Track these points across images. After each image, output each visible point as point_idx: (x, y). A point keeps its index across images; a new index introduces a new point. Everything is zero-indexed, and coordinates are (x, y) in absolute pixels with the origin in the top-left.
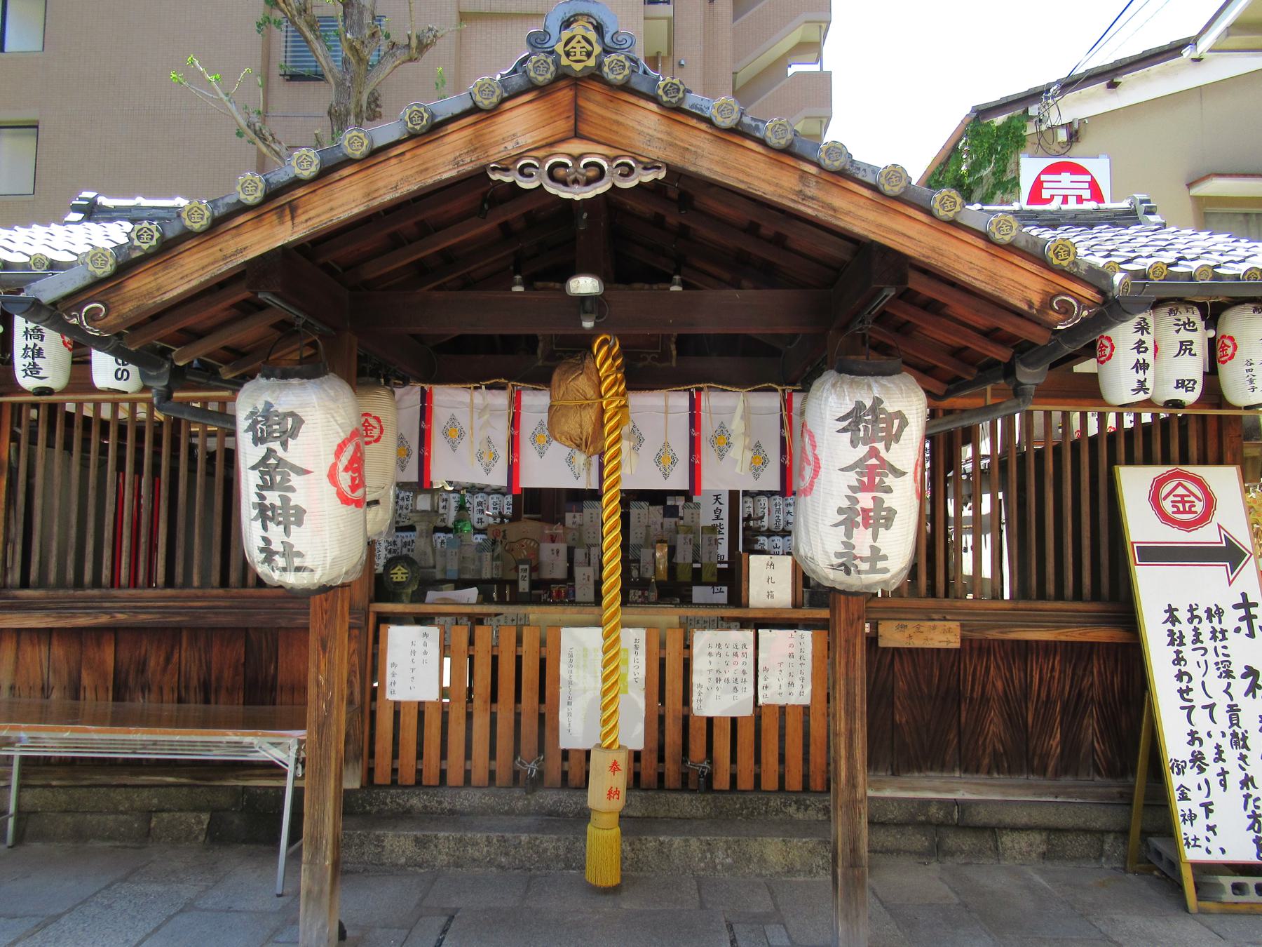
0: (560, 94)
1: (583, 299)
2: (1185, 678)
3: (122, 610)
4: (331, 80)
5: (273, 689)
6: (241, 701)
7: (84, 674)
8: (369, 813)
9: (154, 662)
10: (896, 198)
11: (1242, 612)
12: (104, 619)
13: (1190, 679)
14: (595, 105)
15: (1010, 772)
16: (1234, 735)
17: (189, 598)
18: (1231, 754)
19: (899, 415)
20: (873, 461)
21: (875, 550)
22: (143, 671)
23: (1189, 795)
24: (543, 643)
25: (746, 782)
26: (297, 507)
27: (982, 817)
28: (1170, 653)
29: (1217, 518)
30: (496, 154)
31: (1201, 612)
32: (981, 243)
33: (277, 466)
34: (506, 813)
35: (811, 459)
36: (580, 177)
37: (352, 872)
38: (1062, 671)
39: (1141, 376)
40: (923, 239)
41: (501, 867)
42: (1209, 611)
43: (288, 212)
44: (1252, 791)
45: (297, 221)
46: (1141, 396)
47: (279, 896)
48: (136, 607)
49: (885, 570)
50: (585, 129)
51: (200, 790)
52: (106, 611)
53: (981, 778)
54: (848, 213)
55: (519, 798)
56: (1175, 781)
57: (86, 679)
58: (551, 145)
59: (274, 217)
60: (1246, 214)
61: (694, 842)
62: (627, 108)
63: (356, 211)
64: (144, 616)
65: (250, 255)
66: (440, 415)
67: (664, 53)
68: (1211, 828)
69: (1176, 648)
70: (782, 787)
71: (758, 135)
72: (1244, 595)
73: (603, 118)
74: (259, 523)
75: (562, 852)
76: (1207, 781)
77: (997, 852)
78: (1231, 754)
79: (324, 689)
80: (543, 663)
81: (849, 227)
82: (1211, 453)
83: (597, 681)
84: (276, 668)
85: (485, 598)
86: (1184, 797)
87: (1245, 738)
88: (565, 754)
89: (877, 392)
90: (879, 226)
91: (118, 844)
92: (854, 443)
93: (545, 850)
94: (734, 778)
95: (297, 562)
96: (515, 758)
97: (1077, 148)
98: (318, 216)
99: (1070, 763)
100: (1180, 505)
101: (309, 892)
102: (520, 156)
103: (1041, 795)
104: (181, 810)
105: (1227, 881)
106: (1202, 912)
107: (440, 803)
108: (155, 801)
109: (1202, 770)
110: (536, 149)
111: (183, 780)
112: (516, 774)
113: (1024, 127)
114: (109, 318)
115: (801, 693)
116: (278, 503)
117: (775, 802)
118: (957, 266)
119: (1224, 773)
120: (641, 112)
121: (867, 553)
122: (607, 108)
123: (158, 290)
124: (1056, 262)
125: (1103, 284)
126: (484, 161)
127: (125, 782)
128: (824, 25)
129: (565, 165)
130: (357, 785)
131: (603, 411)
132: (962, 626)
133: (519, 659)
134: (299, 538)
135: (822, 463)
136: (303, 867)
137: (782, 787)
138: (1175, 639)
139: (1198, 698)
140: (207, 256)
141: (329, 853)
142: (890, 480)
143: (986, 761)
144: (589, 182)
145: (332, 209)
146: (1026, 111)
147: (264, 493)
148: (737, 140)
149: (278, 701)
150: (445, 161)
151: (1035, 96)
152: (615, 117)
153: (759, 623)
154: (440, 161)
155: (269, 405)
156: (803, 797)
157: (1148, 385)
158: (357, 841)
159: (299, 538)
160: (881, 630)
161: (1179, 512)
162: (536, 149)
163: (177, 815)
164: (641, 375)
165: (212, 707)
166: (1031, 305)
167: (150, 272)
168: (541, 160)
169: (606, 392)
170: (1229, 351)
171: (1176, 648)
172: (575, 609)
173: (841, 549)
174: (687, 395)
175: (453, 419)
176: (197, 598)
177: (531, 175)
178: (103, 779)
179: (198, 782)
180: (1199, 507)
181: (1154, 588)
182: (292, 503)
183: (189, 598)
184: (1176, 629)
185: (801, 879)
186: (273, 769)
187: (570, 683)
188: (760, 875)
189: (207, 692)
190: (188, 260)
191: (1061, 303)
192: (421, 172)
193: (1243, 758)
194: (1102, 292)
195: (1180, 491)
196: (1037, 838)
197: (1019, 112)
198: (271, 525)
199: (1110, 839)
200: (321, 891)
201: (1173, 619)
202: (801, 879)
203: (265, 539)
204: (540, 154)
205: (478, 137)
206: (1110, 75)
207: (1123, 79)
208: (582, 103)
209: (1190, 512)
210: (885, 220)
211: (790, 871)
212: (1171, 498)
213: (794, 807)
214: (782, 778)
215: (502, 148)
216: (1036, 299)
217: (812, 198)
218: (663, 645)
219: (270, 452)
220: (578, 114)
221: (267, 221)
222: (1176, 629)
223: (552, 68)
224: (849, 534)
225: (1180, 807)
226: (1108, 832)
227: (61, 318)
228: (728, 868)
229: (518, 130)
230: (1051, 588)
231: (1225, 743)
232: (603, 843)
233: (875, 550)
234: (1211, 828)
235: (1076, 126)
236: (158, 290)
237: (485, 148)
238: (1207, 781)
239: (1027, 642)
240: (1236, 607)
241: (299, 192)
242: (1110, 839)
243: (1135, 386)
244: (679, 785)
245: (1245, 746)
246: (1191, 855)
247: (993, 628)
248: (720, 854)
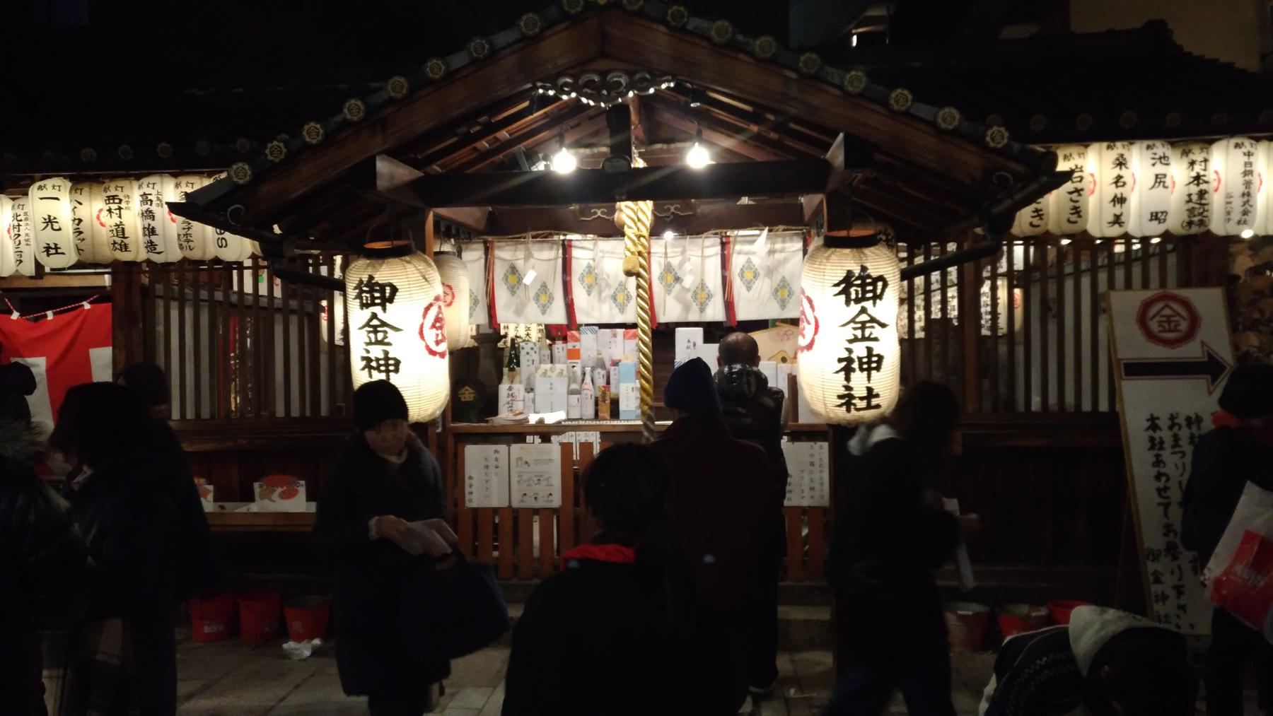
2: (1164, 479)
13: (1168, 480)
19: (881, 278)
21: (870, 390)
23: (1163, 579)
28: (1150, 456)
29: (1202, 335)
31: (1181, 420)
49: (878, 406)
56: (1151, 566)
69: (1155, 452)
76: (1180, 568)
92: (848, 302)
100: (1166, 325)
110: (571, 67)
121: (864, 394)
142: (877, 331)
161: (1164, 331)
162: (571, 67)
171: (1155, 452)
180: (1184, 326)
184: (1158, 435)
195: (1167, 312)
209: (1175, 330)
212: (1158, 318)
219: (374, 316)
222: (1158, 435)
224: (848, 379)
225: (1156, 589)
233: (870, 390)
238: (1180, 568)
243: (1111, 219)
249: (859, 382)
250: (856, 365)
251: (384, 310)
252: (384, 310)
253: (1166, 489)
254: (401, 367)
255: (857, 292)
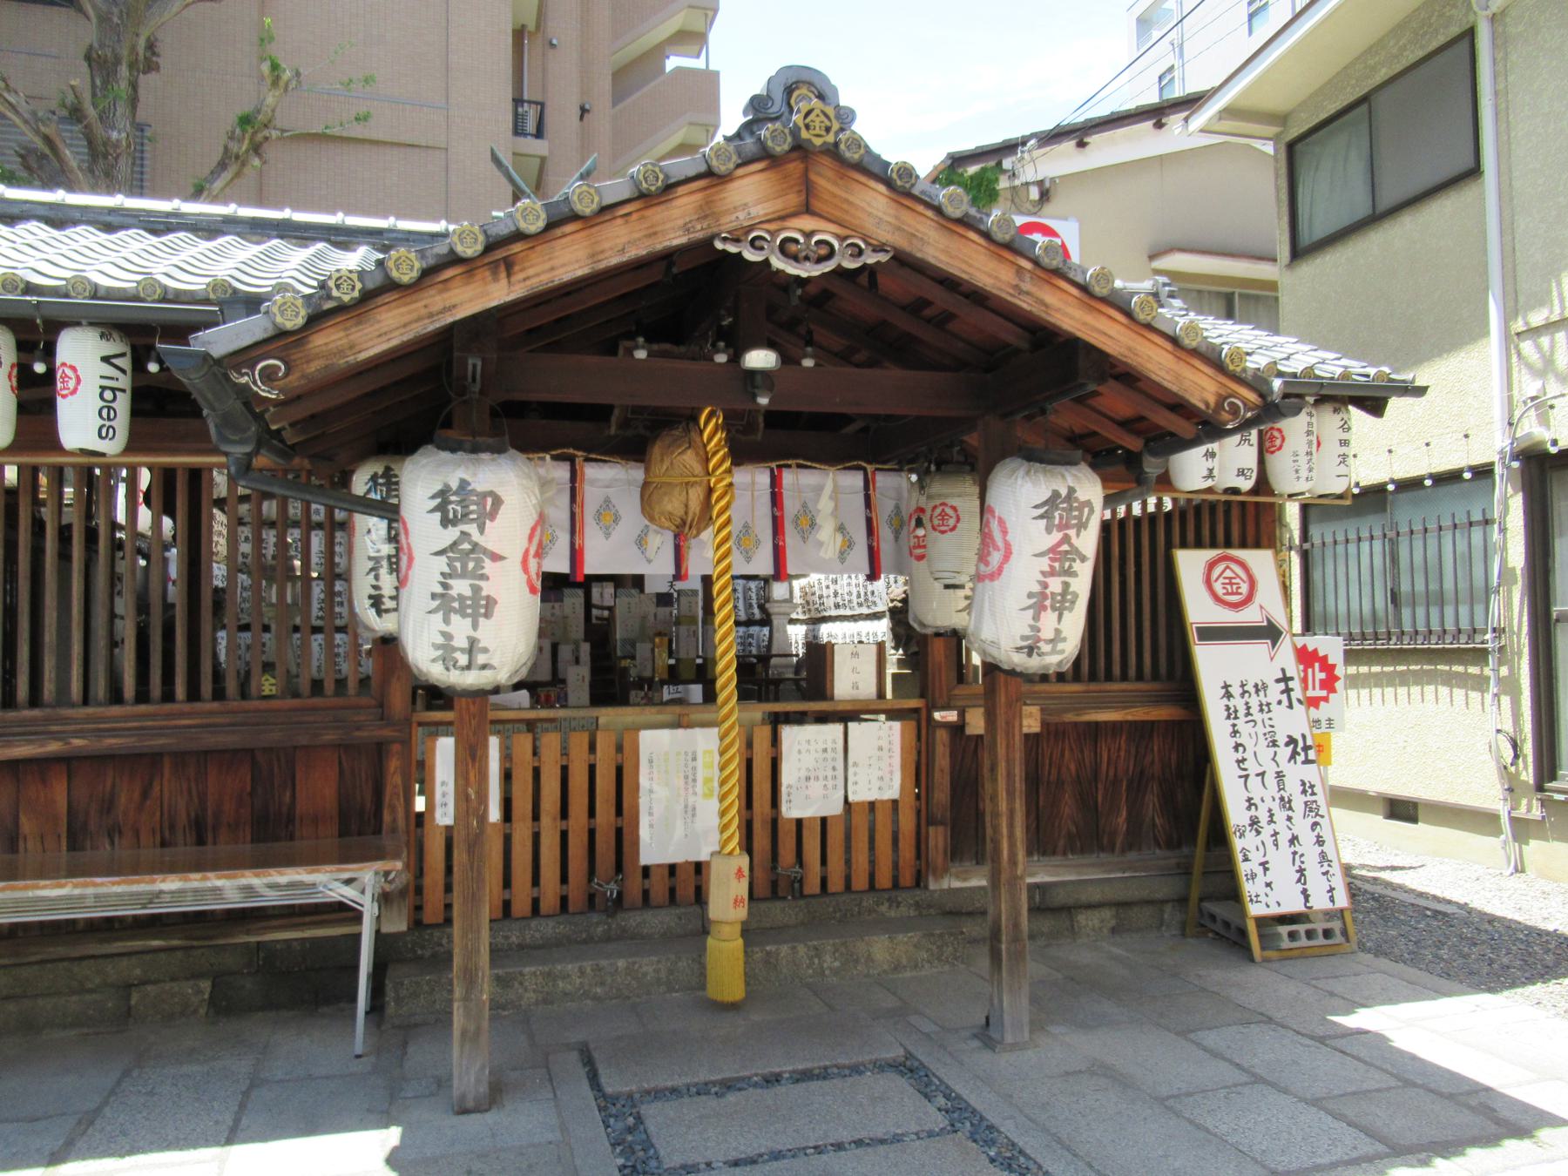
0: (791, 166)
1: (752, 373)
3: (78, 734)
4: (91, 12)
5: (291, 819)
6: (249, 838)
7: (23, 819)
8: (421, 958)
9: (126, 797)
10: (1103, 300)
11: (1282, 686)
12: (53, 747)
14: (825, 179)
15: (1082, 851)
16: (1282, 799)
17: (170, 716)
18: (1280, 816)
20: (1065, 547)
22: (109, 810)
24: (619, 748)
25: (836, 884)
26: (488, 598)
27: (1060, 898)
29: (1259, 598)
30: (728, 223)
31: (1250, 688)
32: (1169, 346)
33: (472, 551)
34: (585, 942)
35: (1000, 544)
36: (811, 255)
37: (416, 1025)
38: (1128, 752)
39: (1210, 464)
40: (1121, 338)
41: (596, 998)
42: (1256, 686)
43: (502, 268)
44: (1298, 848)
45: (513, 279)
46: (1209, 483)
47: (358, 1057)
48: (99, 730)
49: (1062, 652)
50: (817, 205)
51: (200, 951)
52: (55, 736)
53: (1056, 860)
54: (1058, 310)
55: (598, 924)
56: (1238, 844)
57: (27, 825)
58: (783, 218)
59: (488, 273)
60: (1199, 292)
61: (802, 949)
62: (857, 187)
63: (580, 273)
64: (113, 741)
65: (460, 314)
66: (592, 496)
67: (531, 26)
68: (1268, 885)
70: (848, 887)
71: (982, 227)
72: (1283, 670)
73: (835, 196)
74: (440, 615)
75: (663, 975)
77: (1073, 932)
78: (1280, 816)
79: (474, 804)
80: (619, 771)
81: (1059, 323)
82: (1250, 540)
83: (680, 785)
84: (293, 796)
85: (536, 702)
86: (1246, 859)
87: (1290, 801)
88: (646, 871)
89: (1071, 482)
90: (1085, 324)
91: (85, 1030)
92: (1049, 530)
93: (645, 975)
94: (824, 882)
95: (481, 659)
96: (590, 880)
97: (1048, 209)
98: (537, 275)
99: (1134, 840)
101: (464, 1033)
102: (751, 228)
103: (1110, 871)
104: (173, 979)
105: (1283, 930)
106: (1266, 960)
107: (507, 938)
108: (138, 972)
109: (1258, 833)
110: (769, 221)
111: (175, 943)
112: (591, 898)
113: (997, 180)
114: (290, 378)
115: (890, 787)
116: (468, 592)
117: (868, 901)
118: (1149, 366)
119: (1276, 834)
120: (871, 193)
122: (836, 184)
123: (351, 347)
124: (1231, 367)
125: (1264, 388)
126: (715, 230)
127: (91, 952)
128: (710, 14)
129: (796, 241)
130: (403, 927)
131: (710, 491)
132: (1042, 710)
133: (592, 769)
134: (487, 633)
135: (1015, 549)
136: (456, 1005)
137: (872, 886)
138: (1231, 714)
139: (1252, 767)
140: (409, 312)
141: (486, 986)
143: (1061, 843)
144: (820, 260)
145: (552, 269)
146: (999, 164)
147: (449, 581)
148: (961, 230)
149: (297, 834)
150: (673, 227)
151: (1010, 147)
152: (844, 195)
153: (847, 716)
154: (668, 226)
155: (464, 484)
156: (894, 894)
157: (1215, 473)
158: (426, 988)
159: (487, 633)
160: (968, 717)
162: (769, 221)
163: (167, 986)
164: (741, 454)
165: (209, 848)
166: (1207, 405)
167: (341, 326)
168: (773, 234)
169: (715, 469)
170: (1278, 443)
172: (654, 709)
173: (1028, 632)
174: (768, 473)
175: (607, 501)
176: (182, 715)
177: (762, 248)
178: (61, 951)
179: (195, 943)
181: (1214, 666)
182: (484, 593)
183: (170, 716)
184: (1231, 703)
185: (908, 974)
186: (345, 912)
187: (651, 791)
188: (867, 976)
189: (200, 832)
190: (384, 316)
191: (1232, 404)
192: (649, 236)
193: (1289, 819)
194: (1262, 396)
195: (1228, 573)
196: (1107, 914)
197: (992, 163)
198: (455, 618)
199: (1168, 908)
200: (479, 1029)
201: (1228, 695)
202: (908, 974)
203: (444, 634)
204: (772, 227)
205: (708, 202)
206: (1079, 134)
207: (1094, 139)
208: (813, 177)
210: (1090, 319)
211: (897, 968)
212: (1221, 580)
213: (887, 904)
214: (872, 876)
215: (733, 217)
216: (1212, 400)
217: (1028, 293)
218: (749, 745)
220: (808, 189)
221: (479, 277)
222: (1231, 703)
223: (789, 139)
224: (1036, 618)
225: (1243, 868)
226: (1167, 902)
227: (227, 378)
228: (835, 972)
229: (749, 200)
230: (1117, 670)
231: (1275, 806)
232: (726, 954)
234: (1268, 885)
235: (1047, 185)
236: (351, 347)
237: (716, 216)
239: (1097, 723)
240: (1278, 681)
241: (517, 247)
242: (1168, 908)
243: (1205, 473)
244: (768, 893)
245: (1290, 808)
246: (1255, 910)
247: (1066, 711)
248: (828, 958)
249: (1049, 621)
250: (1048, 603)
251: (482, 529)
252: (482, 529)
253: (1244, 760)
254: (497, 610)
255: (1061, 517)
